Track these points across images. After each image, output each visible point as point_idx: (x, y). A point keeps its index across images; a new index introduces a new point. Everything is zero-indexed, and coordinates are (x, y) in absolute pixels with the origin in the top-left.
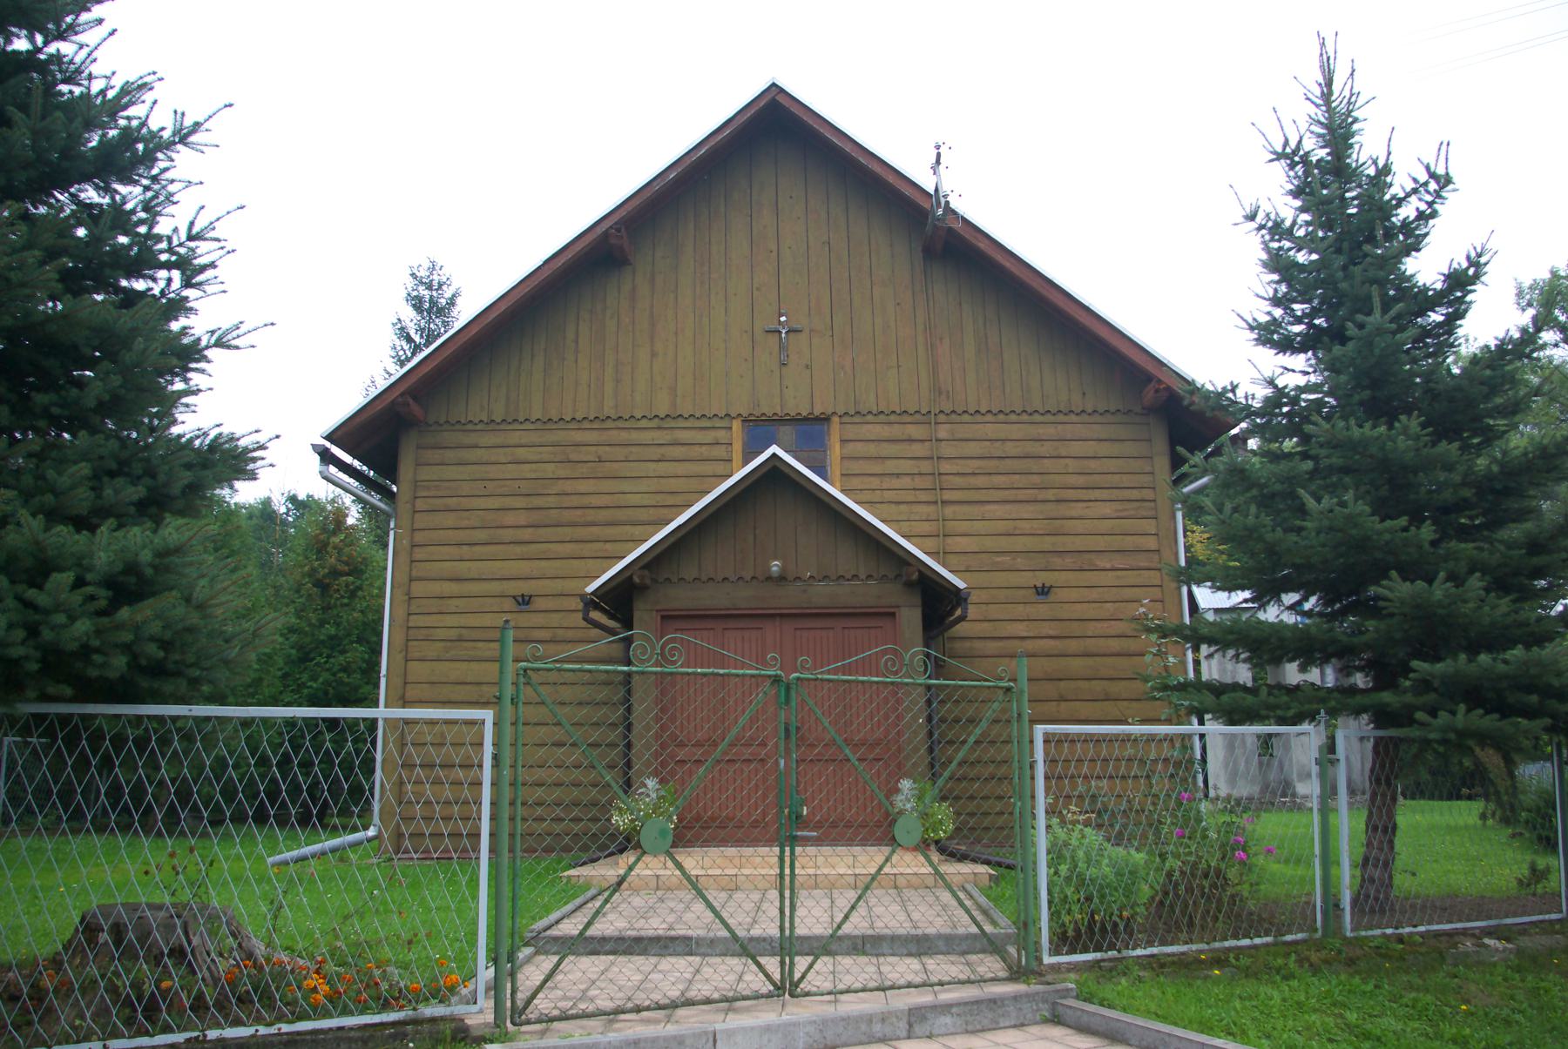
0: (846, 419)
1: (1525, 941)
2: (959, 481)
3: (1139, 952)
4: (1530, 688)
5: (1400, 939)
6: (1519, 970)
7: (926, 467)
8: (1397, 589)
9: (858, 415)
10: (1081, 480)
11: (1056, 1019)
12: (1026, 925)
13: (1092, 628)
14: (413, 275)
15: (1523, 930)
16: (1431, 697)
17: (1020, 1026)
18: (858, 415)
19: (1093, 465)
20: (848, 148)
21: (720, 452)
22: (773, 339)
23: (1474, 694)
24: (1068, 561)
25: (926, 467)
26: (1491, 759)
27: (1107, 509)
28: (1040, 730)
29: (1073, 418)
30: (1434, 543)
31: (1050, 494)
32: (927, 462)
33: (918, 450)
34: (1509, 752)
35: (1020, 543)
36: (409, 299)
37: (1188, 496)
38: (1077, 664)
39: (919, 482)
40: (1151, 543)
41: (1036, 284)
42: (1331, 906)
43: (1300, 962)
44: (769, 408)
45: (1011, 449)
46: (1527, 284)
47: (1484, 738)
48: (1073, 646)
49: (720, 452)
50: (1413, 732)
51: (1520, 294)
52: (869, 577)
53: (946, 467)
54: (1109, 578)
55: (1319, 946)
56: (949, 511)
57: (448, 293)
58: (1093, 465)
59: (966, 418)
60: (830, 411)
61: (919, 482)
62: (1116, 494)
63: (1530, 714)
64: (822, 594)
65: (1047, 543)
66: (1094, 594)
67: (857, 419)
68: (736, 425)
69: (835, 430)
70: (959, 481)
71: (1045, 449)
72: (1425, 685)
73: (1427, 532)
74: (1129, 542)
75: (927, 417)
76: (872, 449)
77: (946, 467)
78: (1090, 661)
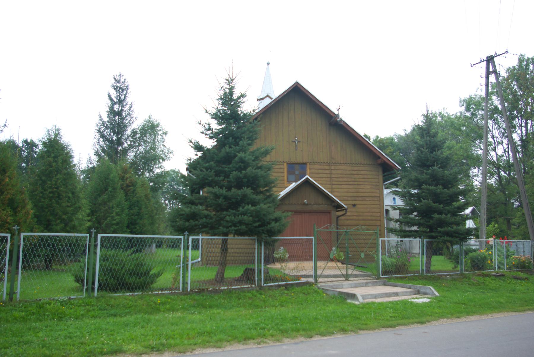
0: (311, 164)
1: (453, 277)
2: (336, 179)
3: (394, 276)
4: (457, 233)
5: (433, 275)
6: (452, 281)
7: (329, 176)
8: (436, 216)
9: (314, 163)
10: (363, 180)
11: (384, 285)
12: (378, 271)
13: (365, 214)
14: (115, 79)
15: (453, 275)
16: (440, 234)
17: (379, 286)
18: (314, 163)
19: (366, 176)
20: (314, 99)
21: (282, 170)
22: (294, 143)
23: (448, 234)
24: (360, 199)
25: (329, 176)
26: (449, 244)
27: (368, 187)
28: (381, 239)
29: (362, 165)
30: (443, 207)
31: (356, 183)
32: (378, 202)
33: (327, 172)
34: (452, 244)
35: (349, 194)
36: (113, 86)
37: (386, 185)
38: (361, 222)
39: (327, 179)
40: (378, 195)
41: (356, 135)
42: (423, 270)
43: (418, 278)
44: (293, 160)
45: (348, 172)
46: (463, 99)
47: (448, 241)
48: (361, 218)
49: (282, 170)
50: (436, 240)
51: (460, 102)
52: (325, 204)
53: (333, 176)
54: (369, 203)
55: (421, 276)
56: (334, 186)
57: (126, 85)
58: (366, 176)
59: (338, 164)
60: (307, 161)
61: (327, 179)
62: (371, 183)
63: (457, 237)
64: (315, 208)
65: (355, 194)
66: (365, 206)
67: (313, 164)
68: (285, 164)
69: (308, 166)
70: (336, 179)
71: (355, 172)
72: (440, 232)
73: (442, 206)
74: (373, 195)
75: (329, 164)
76: (316, 171)
77: (333, 176)
78: (364, 222)
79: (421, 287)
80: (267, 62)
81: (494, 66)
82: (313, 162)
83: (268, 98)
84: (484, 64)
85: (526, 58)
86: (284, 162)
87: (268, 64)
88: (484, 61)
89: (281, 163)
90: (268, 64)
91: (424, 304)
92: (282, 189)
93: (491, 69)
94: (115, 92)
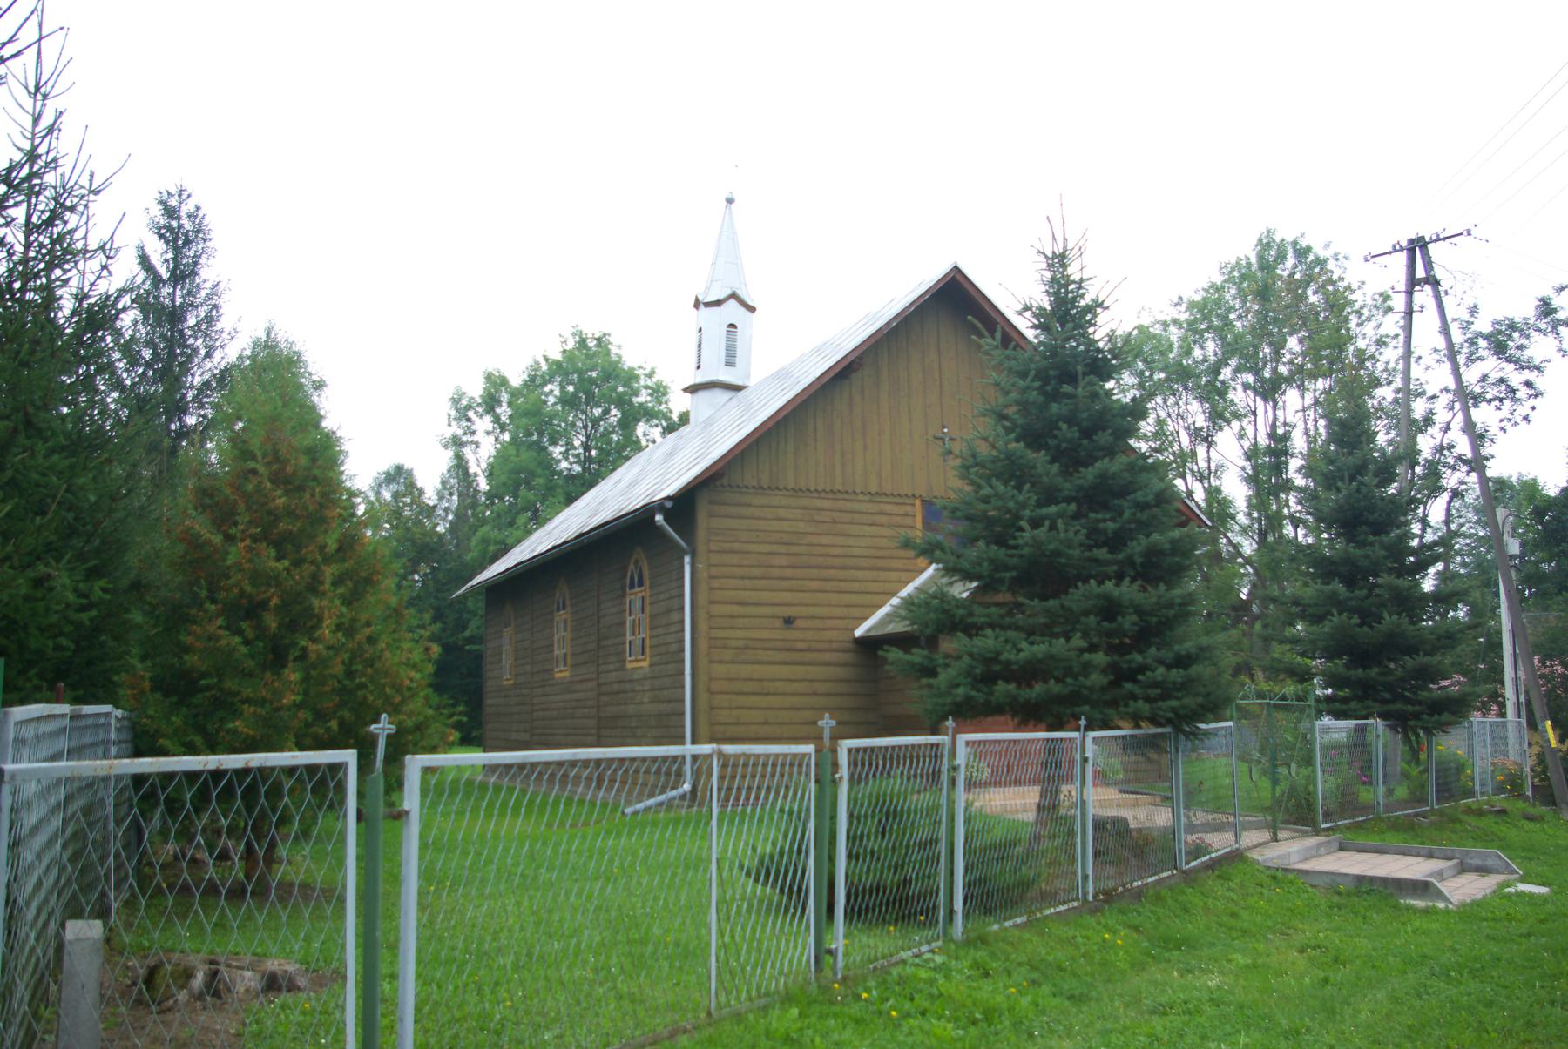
11: (1342, 849)
21: (908, 521)
49: (908, 521)
57: (1377, 297)
68: (918, 502)
79: (1468, 853)
80: (727, 195)
81: (1428, 264)
82: (816, 491)
83: (732, 302)
84: (1402, 257)
85: (1278, 241)
86: (914, 496)
87: (730, 201)
88: (1402, 249)
89: (908, 501)
90: (730, 201)
91: (1542, 895)
92: (912, 574)
93: (1420, 272)
94: (161, 246)
